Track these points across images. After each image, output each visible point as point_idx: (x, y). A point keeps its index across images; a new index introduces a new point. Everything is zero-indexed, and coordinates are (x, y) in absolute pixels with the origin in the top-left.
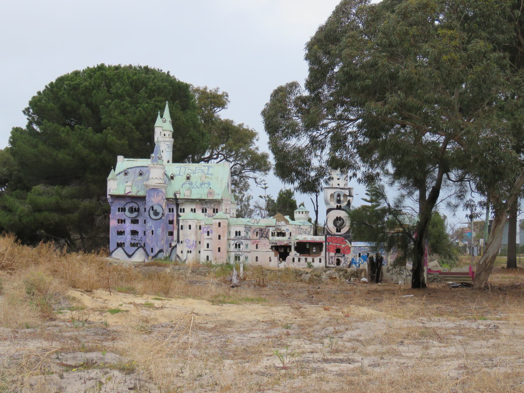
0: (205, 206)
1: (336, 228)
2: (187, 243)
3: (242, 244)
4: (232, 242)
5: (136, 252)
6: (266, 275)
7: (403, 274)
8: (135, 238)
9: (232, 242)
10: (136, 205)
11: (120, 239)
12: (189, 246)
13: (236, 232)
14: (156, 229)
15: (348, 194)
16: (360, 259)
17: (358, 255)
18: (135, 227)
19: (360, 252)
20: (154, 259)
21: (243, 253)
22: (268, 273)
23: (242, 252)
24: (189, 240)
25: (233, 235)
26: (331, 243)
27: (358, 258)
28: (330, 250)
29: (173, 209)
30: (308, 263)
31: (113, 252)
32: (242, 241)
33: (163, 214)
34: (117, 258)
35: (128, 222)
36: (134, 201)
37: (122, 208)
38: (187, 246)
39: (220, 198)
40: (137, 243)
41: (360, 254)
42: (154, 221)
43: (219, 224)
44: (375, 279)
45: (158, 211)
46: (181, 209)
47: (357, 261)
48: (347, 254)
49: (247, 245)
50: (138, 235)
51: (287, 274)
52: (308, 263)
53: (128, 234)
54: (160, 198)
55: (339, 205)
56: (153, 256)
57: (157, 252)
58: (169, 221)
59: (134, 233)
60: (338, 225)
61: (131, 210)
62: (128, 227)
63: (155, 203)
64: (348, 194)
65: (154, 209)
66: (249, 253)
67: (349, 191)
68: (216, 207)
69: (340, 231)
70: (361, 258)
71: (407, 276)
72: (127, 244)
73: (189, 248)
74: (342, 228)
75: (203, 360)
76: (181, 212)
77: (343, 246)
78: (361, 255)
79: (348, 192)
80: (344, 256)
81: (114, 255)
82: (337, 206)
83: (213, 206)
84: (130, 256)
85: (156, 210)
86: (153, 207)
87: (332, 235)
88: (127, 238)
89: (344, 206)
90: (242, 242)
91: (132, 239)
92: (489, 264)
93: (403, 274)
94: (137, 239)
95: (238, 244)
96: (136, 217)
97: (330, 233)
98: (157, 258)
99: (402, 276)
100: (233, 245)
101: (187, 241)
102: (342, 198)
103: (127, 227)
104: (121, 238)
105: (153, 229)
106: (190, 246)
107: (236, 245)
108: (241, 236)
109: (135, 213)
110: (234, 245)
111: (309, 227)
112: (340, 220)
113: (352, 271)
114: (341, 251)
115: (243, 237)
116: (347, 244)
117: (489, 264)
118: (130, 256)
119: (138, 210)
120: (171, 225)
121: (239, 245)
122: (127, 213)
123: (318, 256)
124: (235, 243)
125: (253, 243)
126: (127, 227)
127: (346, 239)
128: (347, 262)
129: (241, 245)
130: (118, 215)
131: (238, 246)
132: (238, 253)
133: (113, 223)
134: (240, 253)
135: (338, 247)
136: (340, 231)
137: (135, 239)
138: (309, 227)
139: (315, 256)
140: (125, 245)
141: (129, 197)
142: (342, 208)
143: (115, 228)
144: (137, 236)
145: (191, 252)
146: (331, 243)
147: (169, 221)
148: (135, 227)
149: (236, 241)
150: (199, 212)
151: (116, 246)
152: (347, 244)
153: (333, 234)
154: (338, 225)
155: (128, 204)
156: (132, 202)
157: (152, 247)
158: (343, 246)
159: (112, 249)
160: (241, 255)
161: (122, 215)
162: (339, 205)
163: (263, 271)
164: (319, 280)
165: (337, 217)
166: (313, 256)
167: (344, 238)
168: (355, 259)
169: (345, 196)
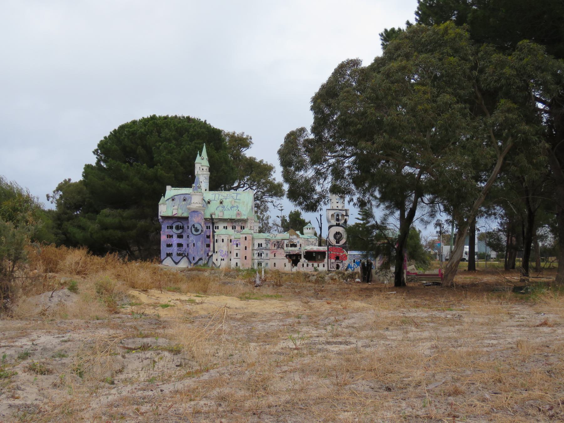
0: (234, 224)
4: (256, 252)
11: (169, 250)
13: (259, 244)
14: (197, 242)
18: (181, 241)
22: (284, 275)
24: (222, 251)
25: (256, 247)
27: (353, 264)
29: (209, 227)
31: (163, 260)
32: (263, 251)
35: (175, 237)
37: (170, 226)
42: (195, 236)
43: (246, 238)
46: (216, 227)
47: (353, 266)
58: (207, 236)
59: (180, 245)
62: (175, 241)
63: (196, 222)
67: (346, 212)
68: (243, 225)
69: (339, 243)
72: (174, 254)
73: (223, 256)
76: (216, 229)
77: (342, 254)
80: (342, 262)
81: (164, 262)
82: (337, 223)
84: (176, 263)
85: (197, 228)
86: (194, 225)
91: (178, 250)
102: (340, 217)
104: (170, 249)
105: (194, 242)
107: (259, 254)
118: (176, 263)
119: (182, 228)
122: (174, 230)
125: (272, 253)
131: (260, 255)
132: (260, 260)
133: (163, 238)
136: (339, 243)
137: (180, 250)
139: (320, 262)
141: (176, 217)
147: (207, 236)
148: (181, 241)
150: (230, 228)
151: (166, 256)
154: (337, 238)
156: (178, 221)
158: (342, 254)
159: (162, 258)
162: (338, 223)
165: (337, 232)
169: (343, 215)
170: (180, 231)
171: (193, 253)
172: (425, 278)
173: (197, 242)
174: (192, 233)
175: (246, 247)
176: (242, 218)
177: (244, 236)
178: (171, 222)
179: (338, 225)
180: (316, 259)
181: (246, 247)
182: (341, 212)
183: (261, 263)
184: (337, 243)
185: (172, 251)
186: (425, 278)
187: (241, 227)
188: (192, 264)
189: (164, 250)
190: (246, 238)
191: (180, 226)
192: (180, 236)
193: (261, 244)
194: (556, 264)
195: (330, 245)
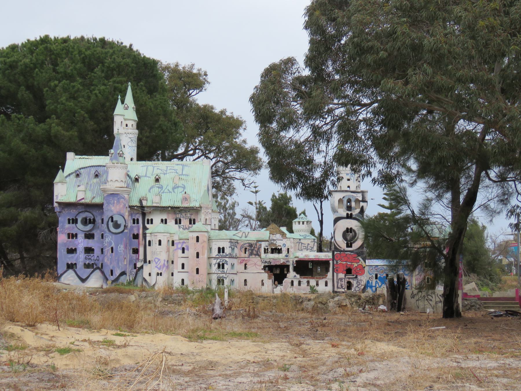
0: (179, 216)
1: (346, 242)
2: (156, 263)
3: (227, 264)
4: (214, 261)
5: (92, 275)
6: (257, 303)
7: (431, 300)
8: (90, 257)
9: (214, 261)
11: (71, 259)
12: (159, 266)
13: (219, 248)
14: (117, 245)
15: (360, 199)
16: (376, 281)
17: (374, 276)
18: (90, 243)
20: (114, 284)
21: (227, 275)
23: (226, 274)
24: (159, 260)
25: (215, 253)
26: (339, 262)
27: (374, 280)
28: (339, 270)
29: (138, 220)
30: (311, 287)
31: (62, 275)
32: (227, 259)
33: (125, 226)
35: (81, 236)
36: (88, 210)
37: (73, 219)
38: (156, 267)
39: (197, 205)
40: (93, 264)
41: (376, 275)
42: (114, 236)
43: (198, 238)
45: (119, 223)
46: (148, 220)
47: (374, 284)
48: (361, 275)
51: (283, 301)
53: (82, 252)
54: (121, 206)
55: (349, 213)
56: (113, 279)
57: (118, 275)
58: (134, 235)
59: (89, 250)
60: (348, 238)
61: (85, 222)
62: (81, 243)
63: (115, 212)
64: (360, 199)
65: (114, 220)
68: (193, 217)
69: (351, 247)
70: (378, 280)
71: (436, 303)
72: (80, 265)
73: (159, 269)
74: (354, 242)
76: (148, 223)
77: (356, 265)
78: (379, 276)
79: (361, 197)
80: (356, 277)
81: (63, 279)
82: (347, 214)
84: (83, 280)
85: (116, 221)
90: (226, 261)
91: (86, 258)
94: (92, 258)
95: (221, 263)
96: (91, 230)
97: (339, 249)
99: (430, 302)
101: (157, 260)
103: (79, 243)
104: (72, 257)
105: (113, 245)
106: (160, 266)
108: (225, 254)
109: (90, 225)
110: (217, 265)
111: (312, 242)
112: (351, 232)
113: (367, 297)
115: (228, 255)
116: (360, 263)
118: (83, 280)
120: (136, 240)
121: (223, 265)
122: (80, 225)
123: (323, 278)
124: (218, 262)
125: (241, 263)
126: (79, 243)
127: (359, 256)
128: (360, 286)
129: (225, 265)
130: (68, 228)
132: (221, 275)
133: (62, 238)
134: (224, 275)
135: (349, 267)
136: (351, 247)
138: (312, 242)
142: (354, 216)
143: (65, 244)
144: (92, 255)
146: (339, 262)
147: (134, 235)
148: (90, 243)
149: (219, 260)
150: (171, 223)
152: (360, 263)
153: (342, 250)
154: (348, 238)
157: (111, 268)
158: (356, 265)
159: (60, 271)
160: (225, 278)
161: (73, 228)
162: (349, 213)
164: (325, 308)
166: (317, 278)
167: (356, 255)
168: (370, 282)
169: (357, 201)
170: (89, 227)
176: (191, 205)
177: (195, 235)
183: (223, 280)
185: (77, 259)
188: (109, 282)
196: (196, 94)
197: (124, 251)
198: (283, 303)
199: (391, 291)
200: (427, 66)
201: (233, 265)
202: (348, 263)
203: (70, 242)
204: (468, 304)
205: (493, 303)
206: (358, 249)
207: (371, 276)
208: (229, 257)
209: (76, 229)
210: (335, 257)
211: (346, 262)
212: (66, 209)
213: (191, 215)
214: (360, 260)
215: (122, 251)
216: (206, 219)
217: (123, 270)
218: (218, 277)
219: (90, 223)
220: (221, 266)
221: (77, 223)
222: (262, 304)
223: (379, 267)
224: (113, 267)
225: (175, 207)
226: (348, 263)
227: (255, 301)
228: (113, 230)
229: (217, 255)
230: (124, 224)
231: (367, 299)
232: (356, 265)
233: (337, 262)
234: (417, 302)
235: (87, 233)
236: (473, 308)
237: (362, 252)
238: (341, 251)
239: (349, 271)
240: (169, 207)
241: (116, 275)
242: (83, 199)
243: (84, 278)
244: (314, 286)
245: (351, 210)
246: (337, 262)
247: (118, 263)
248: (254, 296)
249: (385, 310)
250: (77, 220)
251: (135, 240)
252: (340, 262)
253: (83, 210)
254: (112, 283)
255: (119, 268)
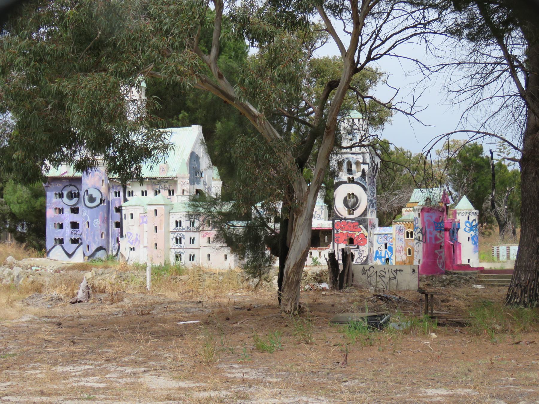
0: (157, 187)
1: (347, 209)
2: (129, 238)
3: (184, 238)
4: (172, 236)
5: (77, 250)
6: (204, 280)
7: (384, 277)
8: (75, 232)
9: (172, 236)
10: (75, 189)
11: (59, 234)
12: (131, 241)
13: (177, 222)
14: (92, 220)
15: (361, 161)
16: (386, 251)
17: (384, 246)
18: (75, 218)
19: (386, 242)
20: (90, 259)
21: (184, 250)
22: (206, 277)
23: (183, 249)
24: (131, 234)
25: (173, 226)
26: (340, 231)
27: (384, 249)
28: (340, 240)
29: (119, 192)
30: (313, 259)
31: (50, 250)
32: (184, 233)
33: (101, 200)
34: (54, 259)
35: (67, 210)
36: (73, 184)
37: (59, 194)
38: (129, 241)
39: (174, 176)
40: (78, 239)
41: (386, 244)
42: (89, 210)
43: (156, 211)
44: (338, 284)
45: (94, 196)
46: (129, 192)
47: (383, 255)
48: (363, 245)
49: (192, 241)
50: (79, 228)
51: (230, 279)
52: (313, 259)
53: (68, 227)
54: (96, 179)
55: (351, 176)
56: (89, 255)
57: (94, 250)
58: (116, 208)
59: (75, 225)
60: (350, 205)
61: (71, 196)
62: (68, 217)
63: (90, 186)
64: (361, 161)
65: (89, 193)
66: (197, 250)
67: (363, 157)
68: (172, 188)
69: (353, 214)
70: (387, 250)
71: (390, 279)
72: (67, 241)
73: (132, 243)
74: (356, 209)
75: (265, 383)
76: (129, 195)
77: (357, 234)
78: (388, 245)
79: (362, 158)
80: (358, 248)
81: (51, 254)
82: (349, 178)
83: (167, 186)
84: (70, 256)
85: (91, 196)
86: (87, 191)
87: (342, 219)
88: (67, 233)
89: (357, 178)
90: (183, 235)
91: (72, 233)
92: (292, 276)
93: (384, 277)
94: (78, 233)
95: (178, 238)
96: (75, 205)
97: (339, 217)
98: (95, 258)
99: (384, 279)
100: (172, 239)
101: (129, 234)
102: (354, 167)
103: (65, 218)
104: (60, 232)
105: (89, 220)
106: (133, 241)
107: (177, 240)
108: (181, 228)
109: (75, 199)
110: (174, 240)
111: (319, 209)
112: (353, 198)
113: (314, 273)
114: (355, 241)
115: (184, 229)
116: (362, 232)
117: (292, 276)
118: (70, 256)
119: (77, 196)
120: (119, 214)
121: (180, 239)
122: (65, 199)
123: (326, 249)
124: (175, 236)
125: (204, 236)
126: (65, 218)
127: (361, 224)
128: (362, 257)
129: (182, 239)
130: (55, 203)
131: (178, 241)
132: (179, 250)
133: (50, 213)
134: (181, 250)
135: (350, 236)
136: (353, 214)
137: (75, 234)
138: (319, 209)
139: (322, 249)
140: (64, 241)
141: (65, 178)
142: (355, 180)
143: (52, 219)
144: (77, 229)
145: (134, 249)
146: (340, 231)
147: (116, 208)
148: (75, 218)
149: (176, 235)
150: (151, 194)
151: (53, 243)
152: (362, 232)
153: (343, 217)
154: (350, 205)
155: (66, 188)
156: (71, 185)
157: (87, 243)
158: (357, 234)
159: (48, 247)
160: (182, 253)
161: (60, 203)
162: (351, 176)
163: (200, 275)
164: (269, 286)
165: (349, 194)
166: (319, 249)
167: (358, 224)
168: (379, 252)
169: (357, 163)
170: (75, 200)
171: (87, 238)
172: (499, 281)
173: (92, 220)
174: (85, 205)
175: (156, 228)
176: (168, 176)
177: (154, 208)
178: (60, 186)
179: (351, 181)
180: (321, 244)
181: (156, 228)
182: (355, 156)
183: (181, 255)
184: (350, 214)
185: (64, 234)
186: (499, 281)
187: (170, 191)
188: (86, 257)
189: (52, 233)
190: (156, 211)
191: (75, 193)
192: (75, 210)
193: (180, 222)
194: (515, 62)
195: (338, 217)
196: (321, 46)
197: (100, 226)
198: (230, 280)
199: (332, 267)
200: (145, 27)
201: (192, 241)
202: (350, 232)
203: (57, 217)
204: (446, 279)
205: (494, 276)
206: (359, 216)
207: (380, 246)
208: (186, 231)
209: (62, 203)
210: (336, 226)
211: (347, 231)
212: (52, 184)
213: (170, 185)
214: (361, 229)
215: (98, 226)
216: (183, 190)
217: (100, 245)
218: (175, 253)
219: (75, 197)
220: (178, 241)
221: (63, 197)
222: (209, 282)
223: (389, 235)
224: (89, 242)
225: (152, 178)
226: (350, 232)
227: (202, 278)
228: (89, 204)
229: (175, 229)
230: (100, 197)
231: (314, 275)
232: (358, 234)
233: (337, 232)
234: (369, 278)
235: (73, 207)
236: (453, 283)
237: (364, 219)
238: (342, 219)
239: (351, 241)
240: (147, 178)
241: (92, 250)
242: (66, 172)
243: (70, 253)
244: (317, 258)
245: (352, 174)
246: (337, 232)
247: (94, 238)
248: (201, 273)
249: (325, 288)
250: (63, 194)
251: (118, 213)
252: (341, 231)
253: (68, 184)
254: (88, 259)
255: (95, 243)
